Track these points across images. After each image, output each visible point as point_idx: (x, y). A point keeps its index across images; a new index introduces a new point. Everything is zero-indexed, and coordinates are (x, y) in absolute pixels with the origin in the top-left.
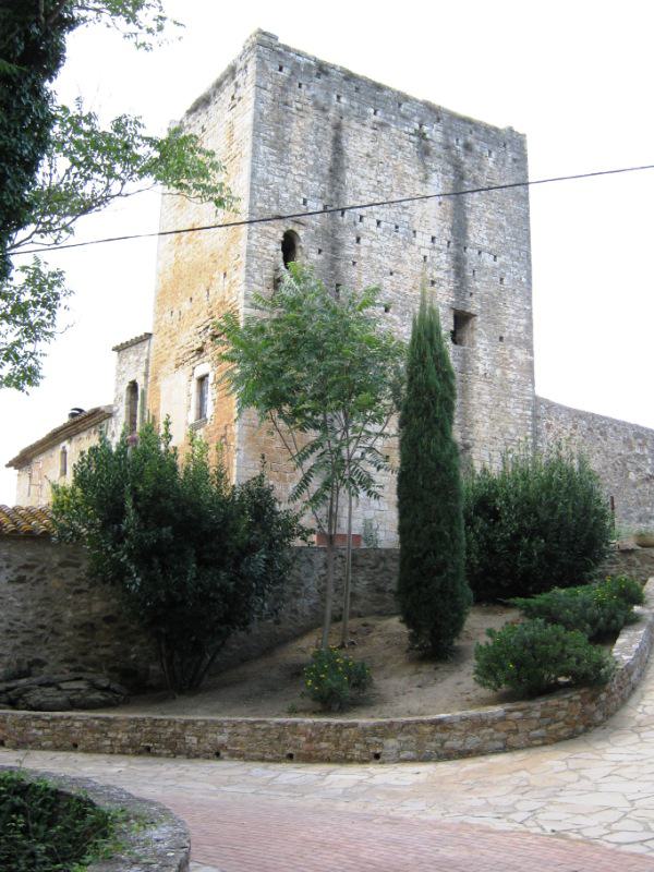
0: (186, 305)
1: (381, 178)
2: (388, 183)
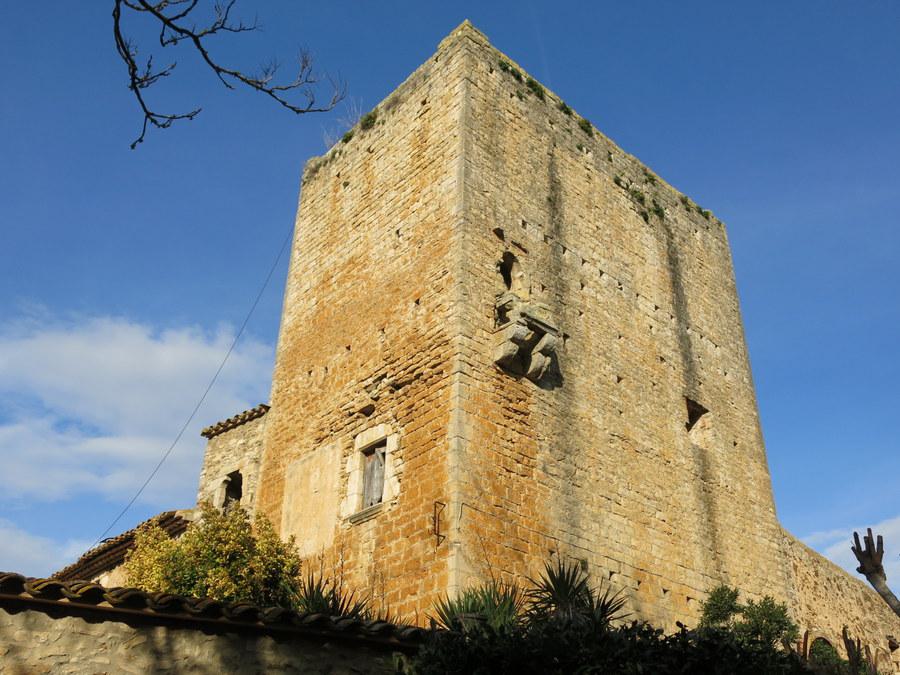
0: (340, 357)
1: (600, 224)
2: (608, 232)
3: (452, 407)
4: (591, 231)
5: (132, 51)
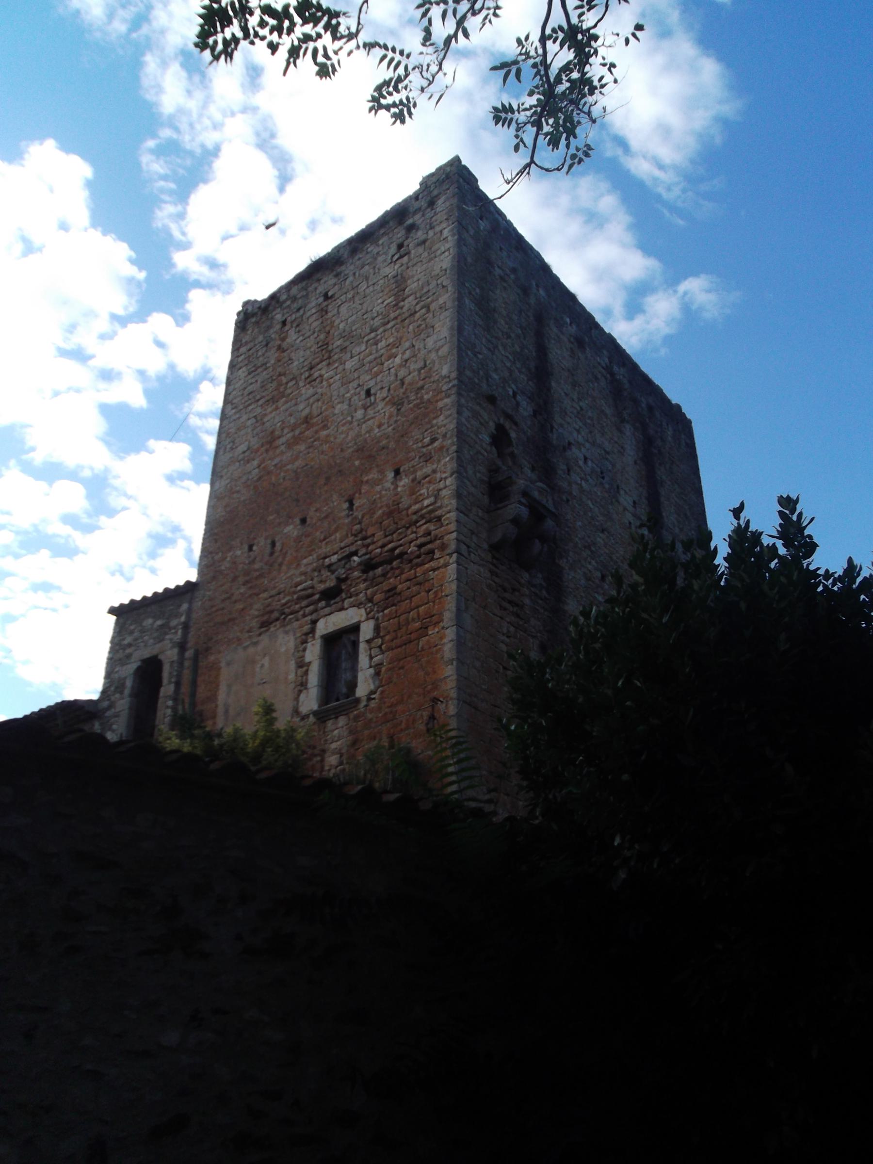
0: (292, 530)
2: (590, 414)
3: (447, 592)
4: (575, 411)
5: (544, 171)
